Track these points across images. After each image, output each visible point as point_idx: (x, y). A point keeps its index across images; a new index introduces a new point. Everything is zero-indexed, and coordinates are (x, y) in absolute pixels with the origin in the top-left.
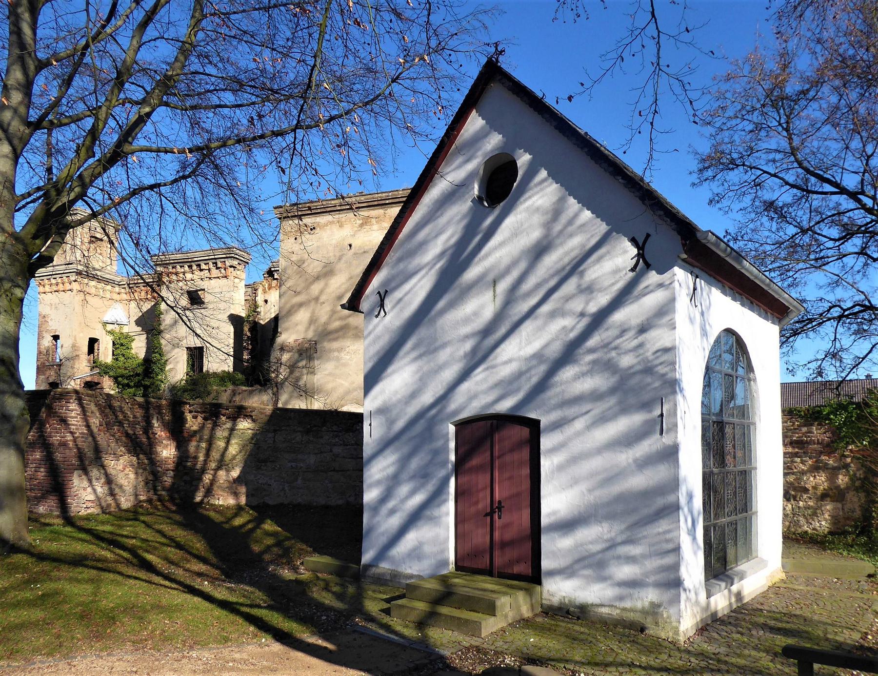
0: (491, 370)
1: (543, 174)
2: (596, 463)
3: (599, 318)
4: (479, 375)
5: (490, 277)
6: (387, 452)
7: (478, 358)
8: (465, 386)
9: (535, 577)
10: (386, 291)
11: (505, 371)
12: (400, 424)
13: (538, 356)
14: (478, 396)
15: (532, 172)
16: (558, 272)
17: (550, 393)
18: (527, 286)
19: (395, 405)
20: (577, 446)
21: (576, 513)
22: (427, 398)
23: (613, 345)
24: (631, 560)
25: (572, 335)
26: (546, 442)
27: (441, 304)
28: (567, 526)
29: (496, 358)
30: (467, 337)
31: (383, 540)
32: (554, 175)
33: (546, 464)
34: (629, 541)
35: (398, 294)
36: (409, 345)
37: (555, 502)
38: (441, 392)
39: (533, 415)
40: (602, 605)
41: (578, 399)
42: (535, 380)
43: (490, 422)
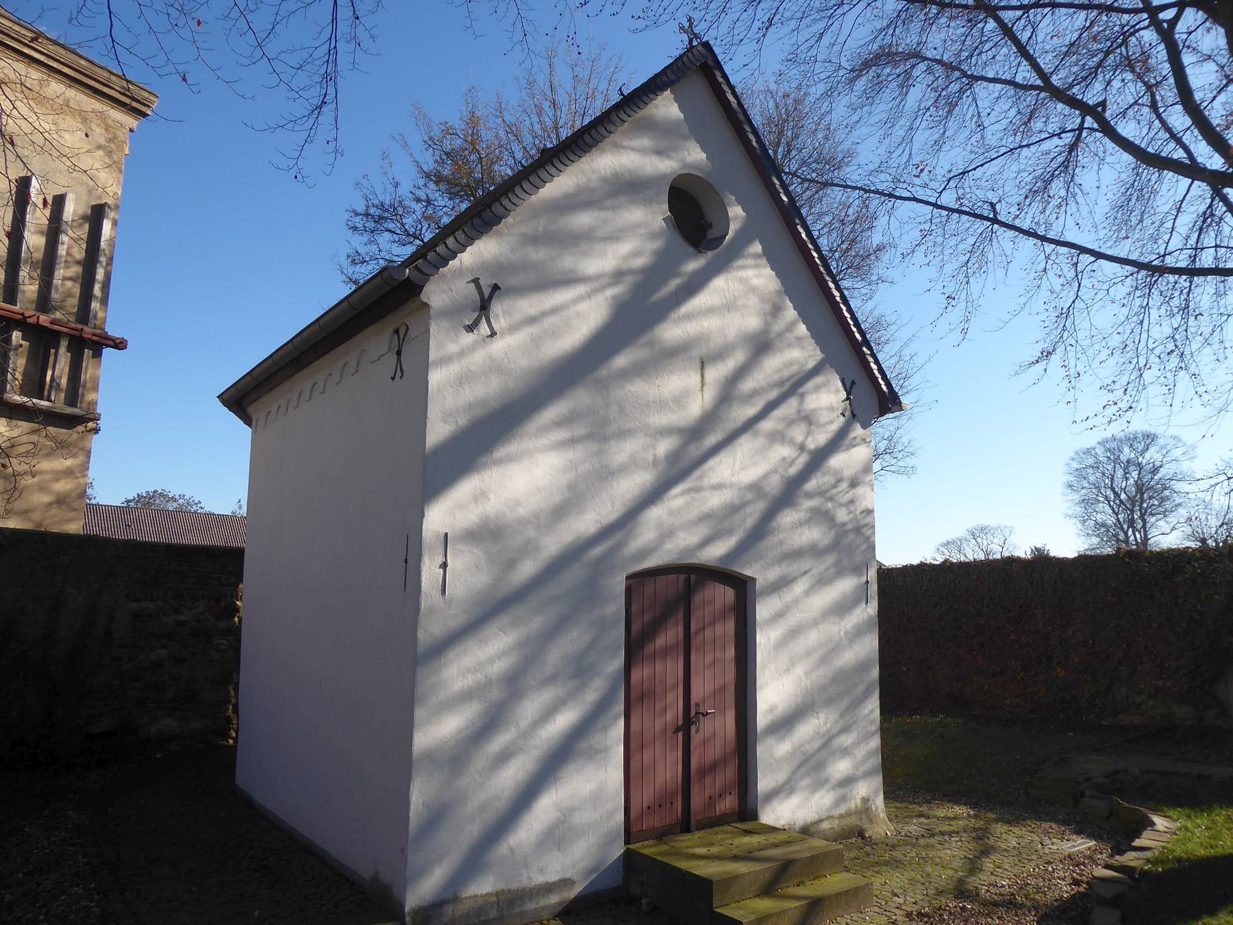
0: (693, 495)
1: (757, 248)
2: (812, 638)
3: (818, 458)
4: (676, 499)
5: (697, 353)
6: (491, 630)
7: (678, 471)
8: (656, 513)
9: (746, 813)
10: (496, 288)
11: (715, 500)
12: (527, 569)
13: (756, 488)
14: (678, 529)
15: (744, 238)
16: (781, 383)
17: (771, 540)
18: (748, 385)
19: (523, 522)
20: (794, 618)
21: (800, 699)
22: (586, 522)
23: (829, 494)
24: (845, 752)
25: (793, 471)
26: (763, 610)
27: (621, 361)
28: (786, 723)
29: (701, 477)
30: (664, 432)
31: (473, 830)
32: (772, 258)
33: (765, 639)
34: (845, 730)
35: (529, 305)
36: (551, 413)
37: (774, 692)
38: (613, 517)
39: (748, 572)
40: (821, 821)
41: (796, 554)
42: (750, 522)
43: (682, 577)
